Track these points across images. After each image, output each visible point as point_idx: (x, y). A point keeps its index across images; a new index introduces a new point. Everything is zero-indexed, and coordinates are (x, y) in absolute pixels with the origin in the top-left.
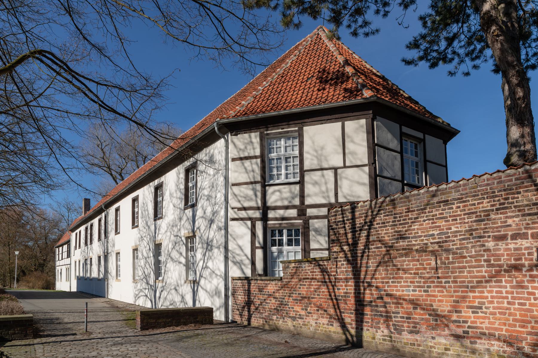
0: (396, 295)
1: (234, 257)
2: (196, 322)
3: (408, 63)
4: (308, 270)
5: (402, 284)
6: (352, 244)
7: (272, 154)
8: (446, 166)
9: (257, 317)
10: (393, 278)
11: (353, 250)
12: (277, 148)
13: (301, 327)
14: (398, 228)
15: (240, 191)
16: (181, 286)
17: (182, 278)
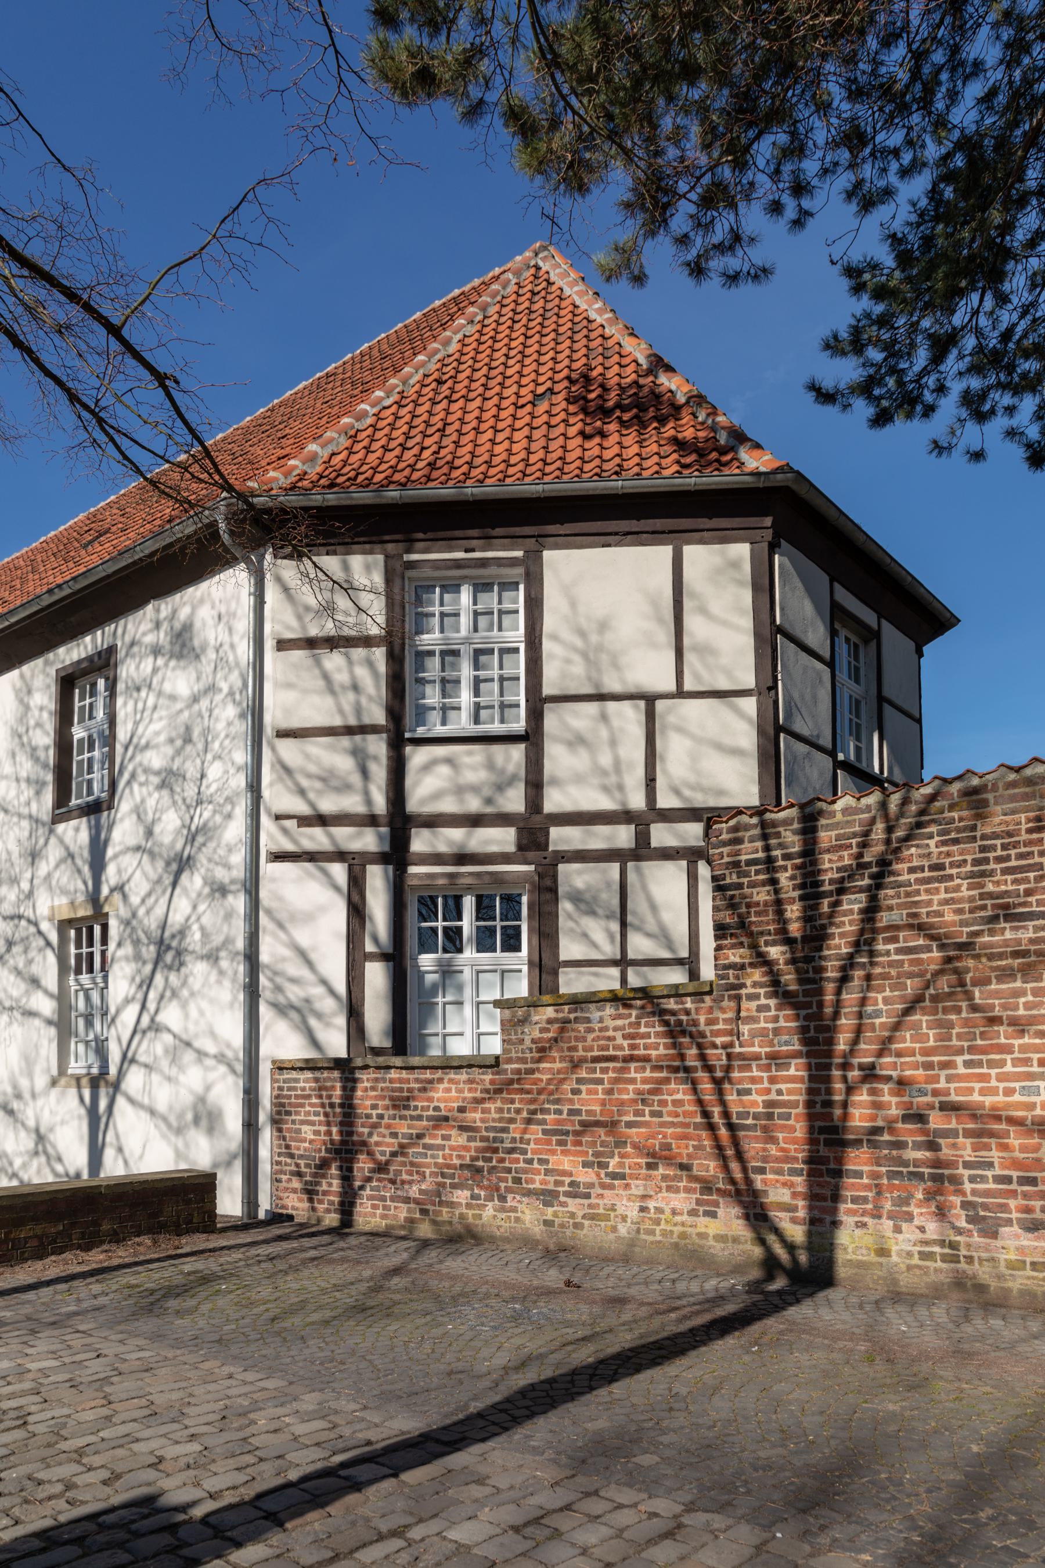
0: (981, 1106)
1: (279, 989)
2: (155, 1229)
3: (825, 396)
4: (615, 1029)
5: (1009, 1068)
6: (805, 939)
7: (425, 636)
8: (919, 721)
9: (383, 1199)
10: (971, 1050)
11: (808, 960)
12: (443, 615)
13: (576, 1226)
14: (998, 883)
15: (307, 756)
16: (34, 1096)
17: (38, 1069)
